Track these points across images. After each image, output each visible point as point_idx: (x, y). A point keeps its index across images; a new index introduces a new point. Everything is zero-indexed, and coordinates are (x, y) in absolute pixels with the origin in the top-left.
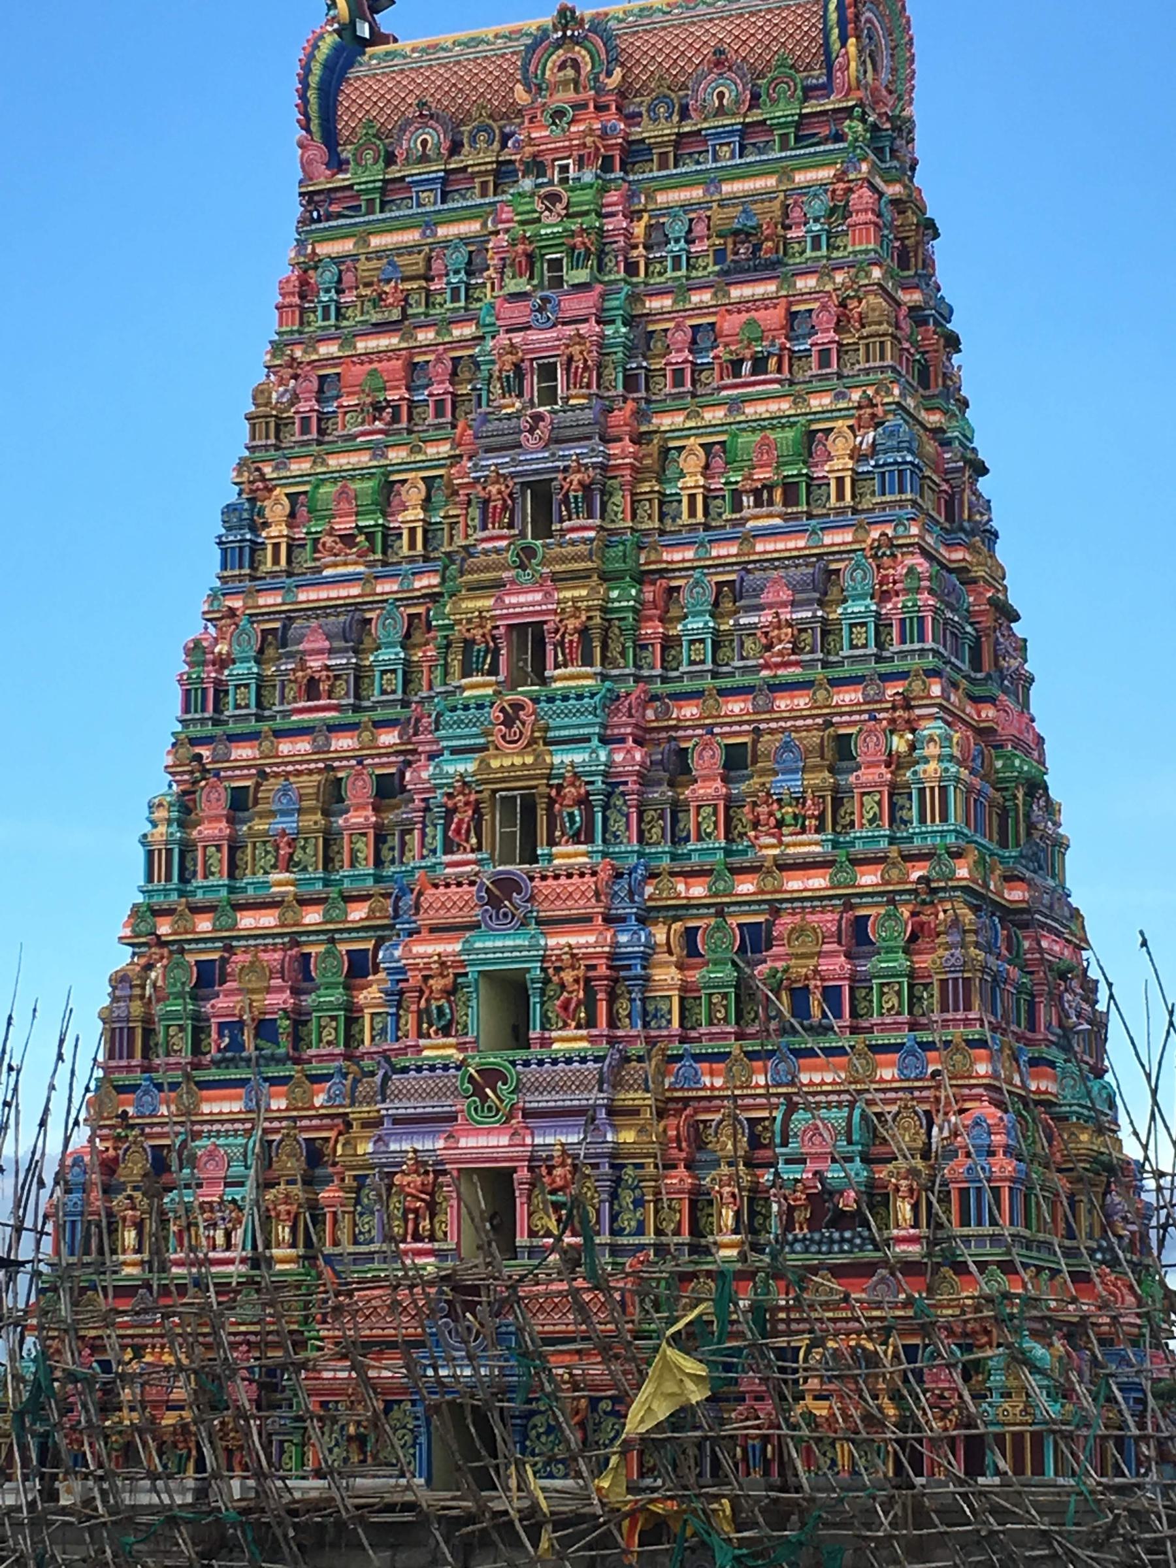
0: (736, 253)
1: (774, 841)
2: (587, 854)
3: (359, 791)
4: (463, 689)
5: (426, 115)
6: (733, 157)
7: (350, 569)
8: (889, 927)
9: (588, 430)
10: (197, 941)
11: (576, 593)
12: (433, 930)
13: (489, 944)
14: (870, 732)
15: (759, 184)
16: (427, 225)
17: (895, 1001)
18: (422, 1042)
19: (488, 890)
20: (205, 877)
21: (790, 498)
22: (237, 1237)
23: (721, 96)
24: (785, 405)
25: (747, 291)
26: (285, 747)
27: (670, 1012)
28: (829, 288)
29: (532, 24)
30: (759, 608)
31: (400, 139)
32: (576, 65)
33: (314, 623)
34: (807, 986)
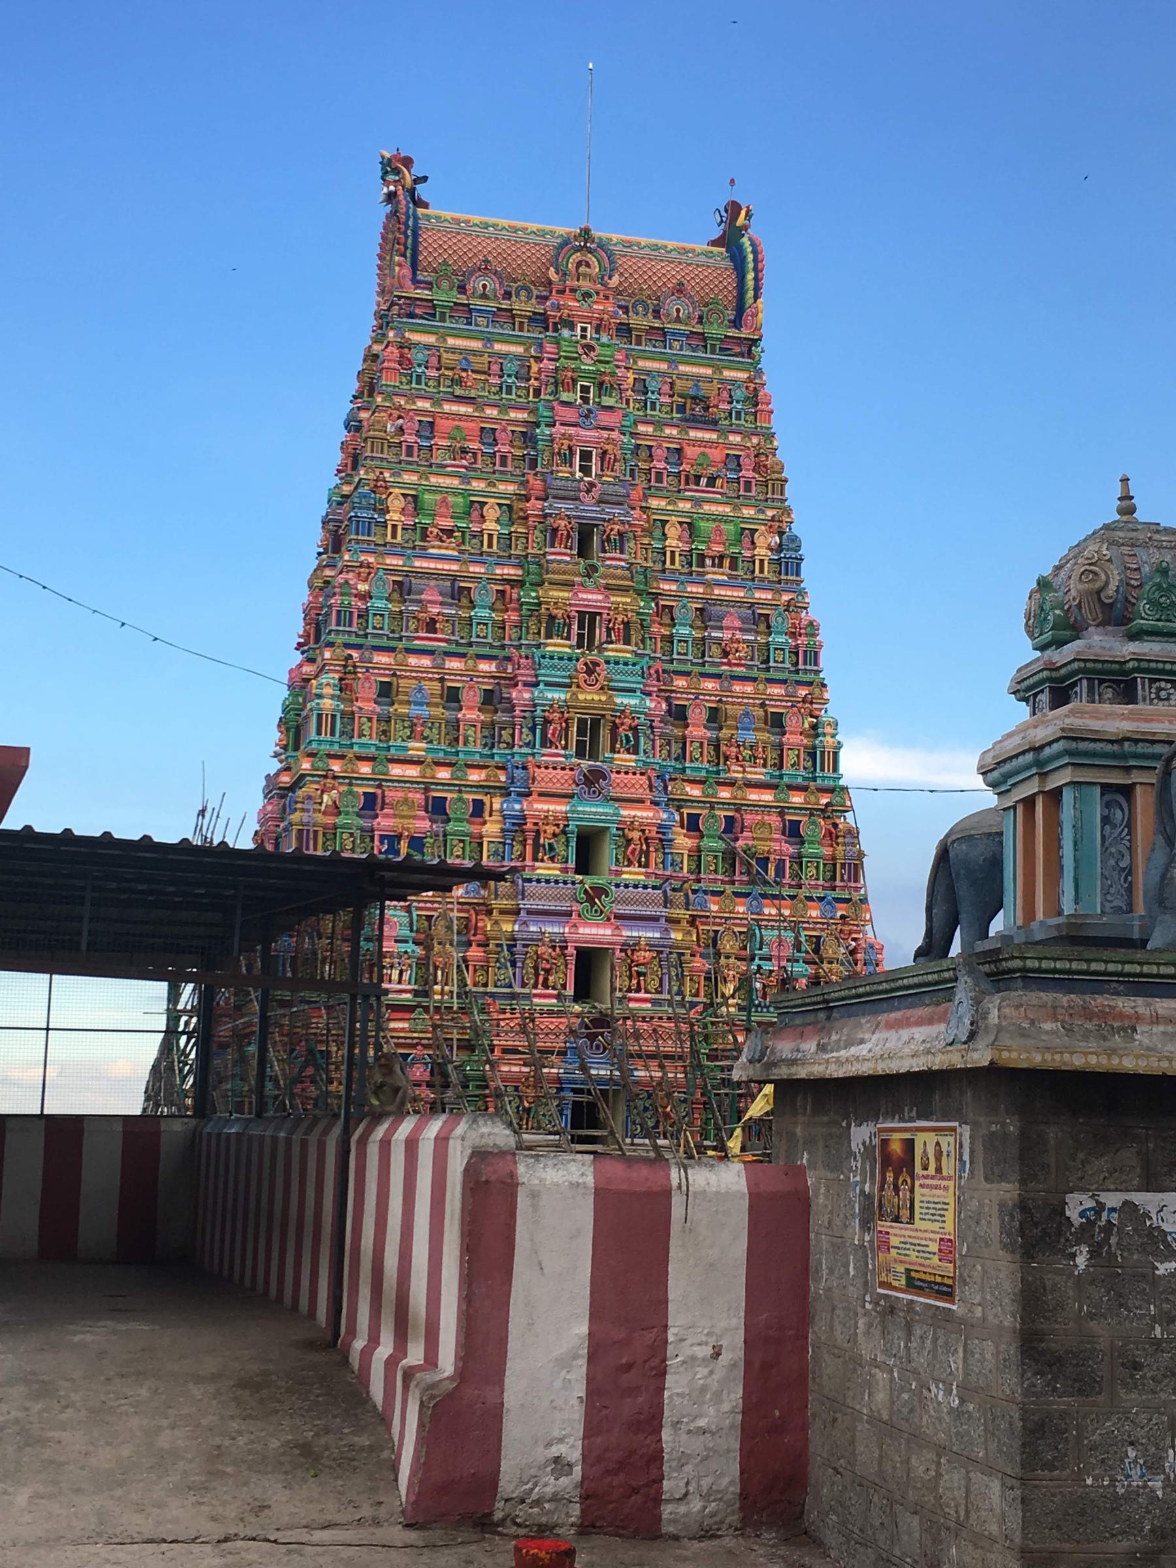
0: (693, 409)
1: (741, 769)
2: (636, 761)
3: (471, 697)
4: (546, 645)
5: (485, 268)
6: (681, 349)
7: (450, 552)
8: (813, 829)
9: (621, 499)
10: (437, 784)
11: (624, 600)
12: (541, 795)
13: (588, 809)
14: (470, 688)
15: (702, 371)
16: (489, 340)
17: (814, 872)
18: (537, 864)
19: (585, 775)
20: (360, 737)
21: (733, 567)
22: (406, 976)
23: (678, 310)
24: (728, 509)
25: (700, 435)
26: (413, 660)
27: (682, 862)
28: (748, 445)
29: (562, 230)
30: (721, 628)
31: (469, 279)
32: (588, 265)
33: (433, 583)
34: (768, 858)
